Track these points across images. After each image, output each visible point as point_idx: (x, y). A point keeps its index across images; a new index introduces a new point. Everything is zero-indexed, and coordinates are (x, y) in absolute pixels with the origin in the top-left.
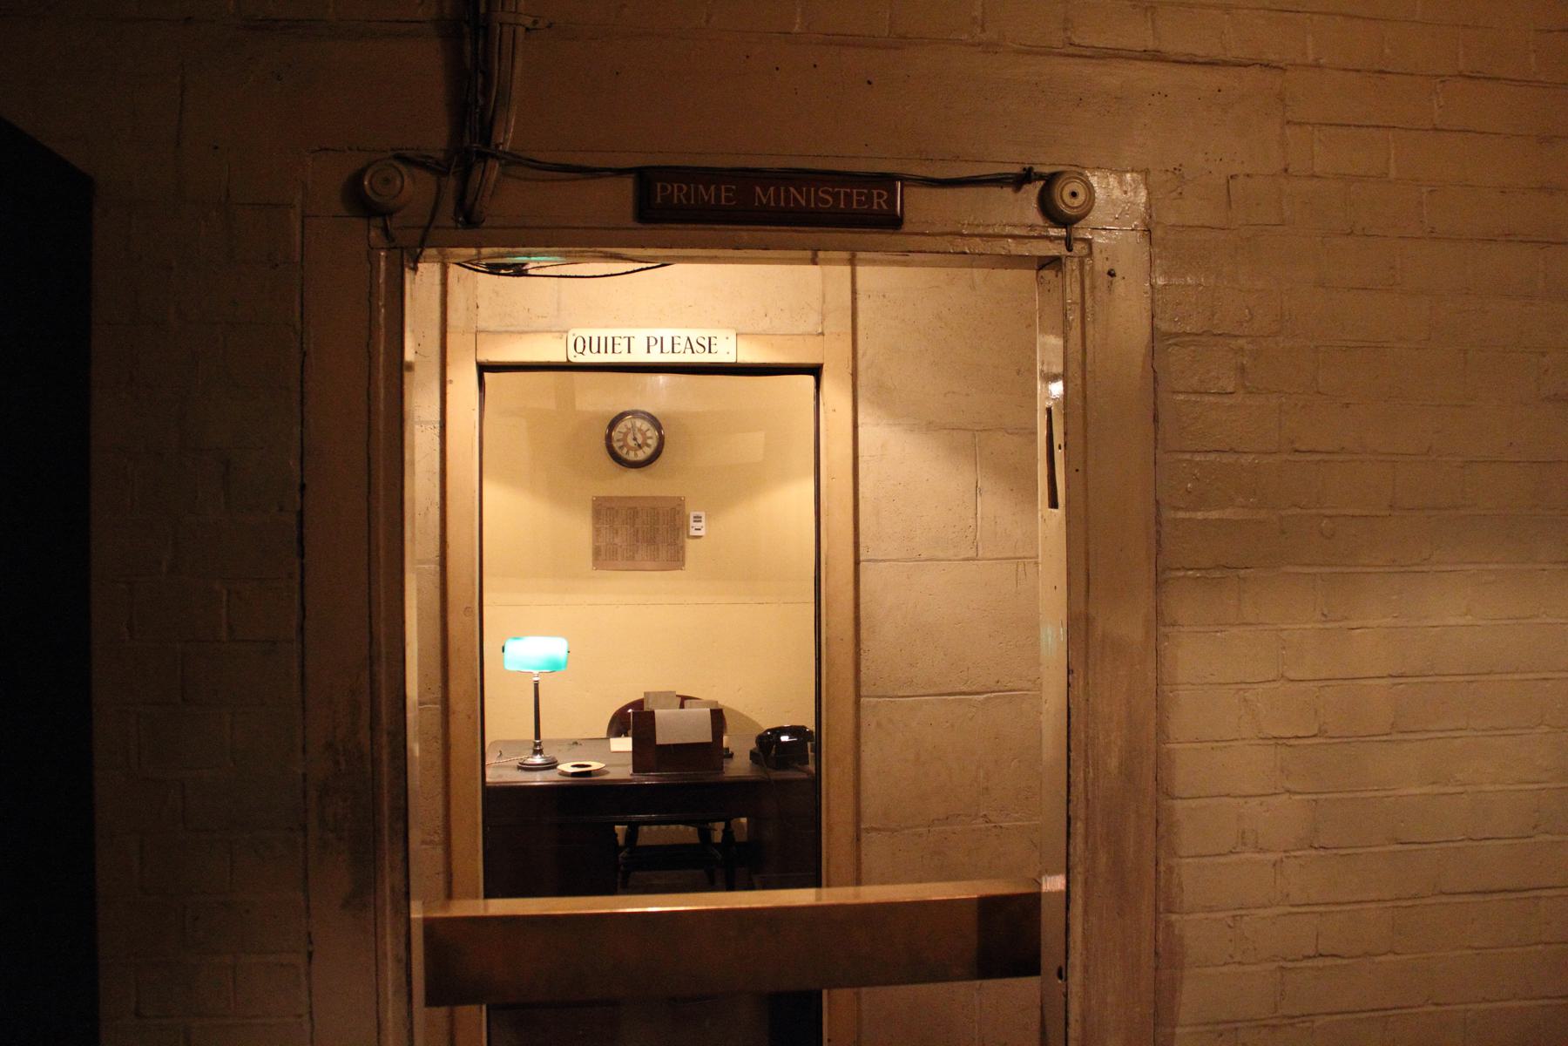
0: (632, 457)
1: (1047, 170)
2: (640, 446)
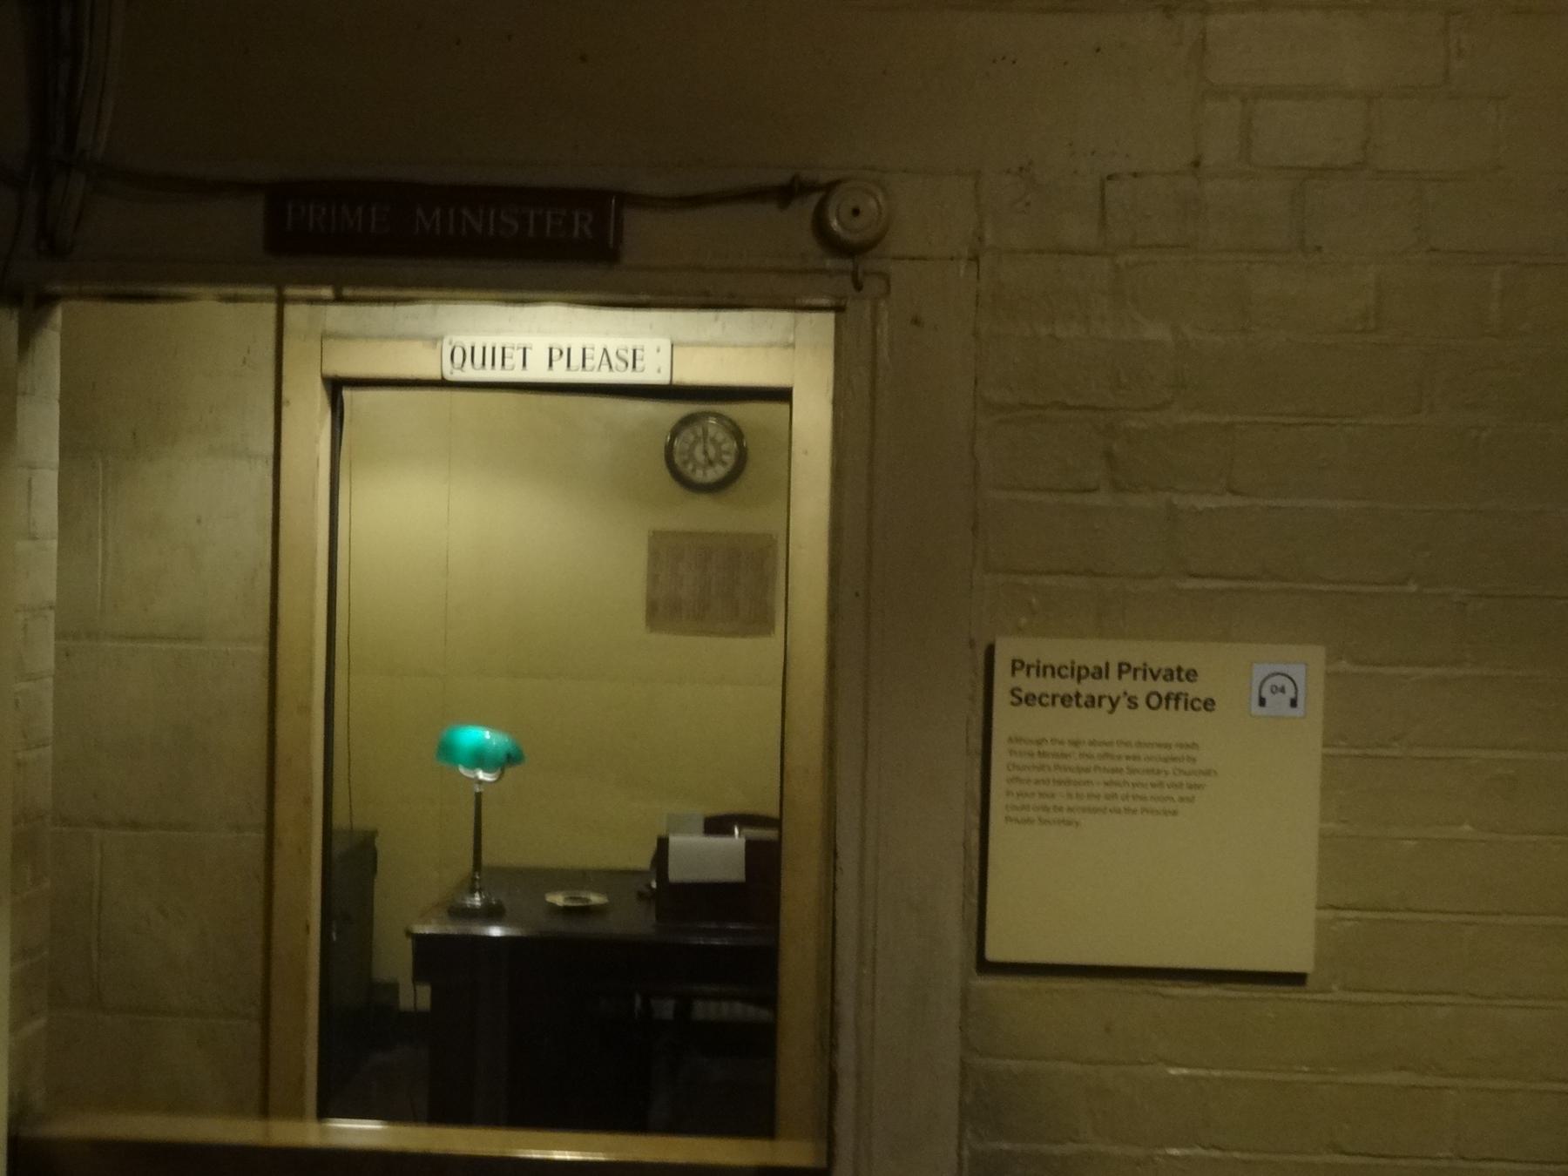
0: (699, 476)
1: (824, 178)
2: (711, 463)
